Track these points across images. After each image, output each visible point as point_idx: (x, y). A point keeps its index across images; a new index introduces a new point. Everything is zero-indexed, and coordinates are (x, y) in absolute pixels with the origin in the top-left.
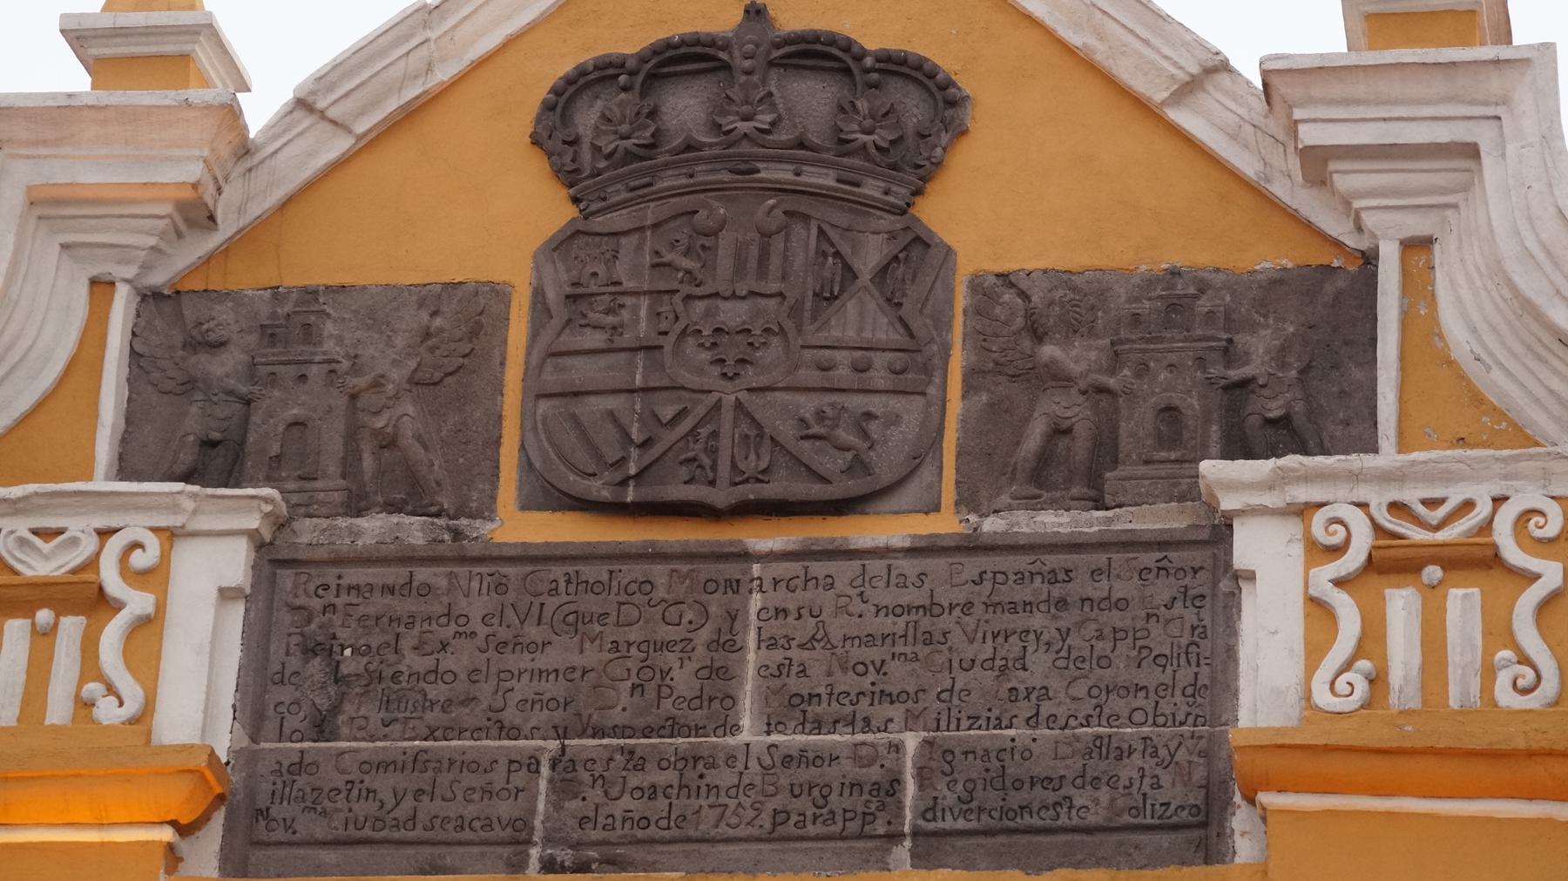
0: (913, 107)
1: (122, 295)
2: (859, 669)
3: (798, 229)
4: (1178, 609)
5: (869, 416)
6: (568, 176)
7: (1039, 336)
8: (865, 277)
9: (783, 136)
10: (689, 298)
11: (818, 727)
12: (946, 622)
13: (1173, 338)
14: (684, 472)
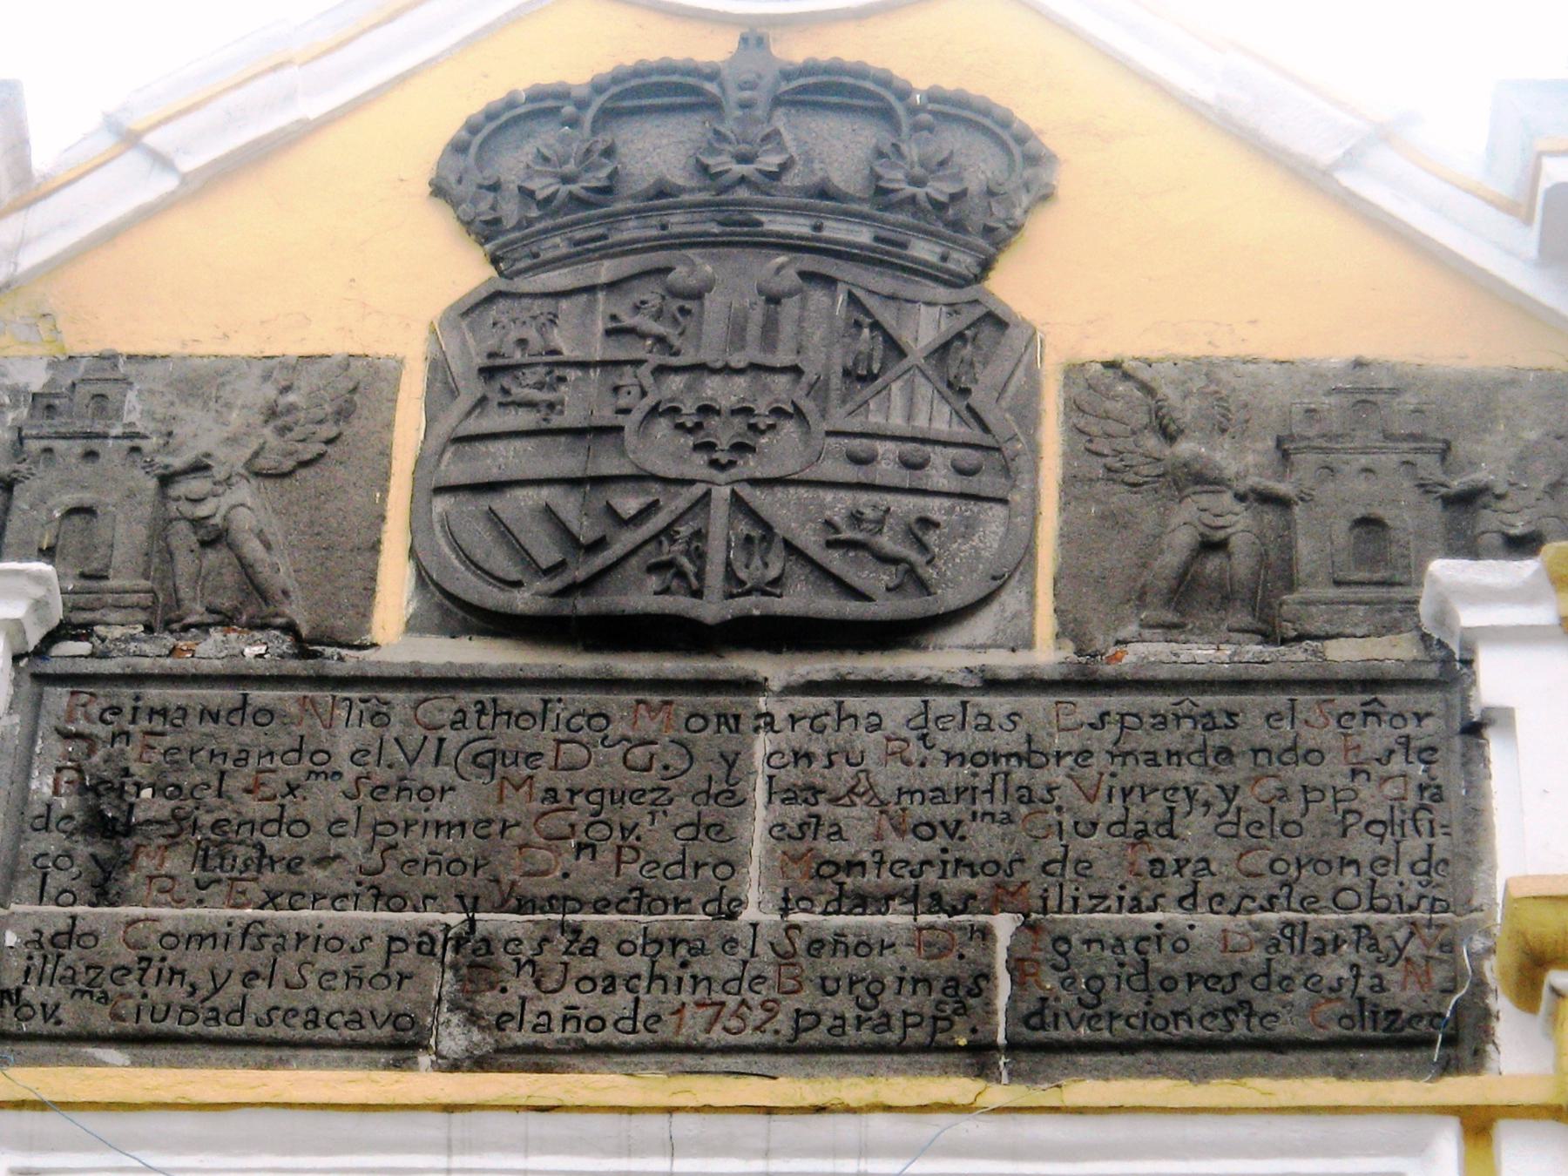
2: (925, 830)
4: (1397, 764)
5: (927, 523)
6: (485, 230)
7: (1169, 437)
11: (862, 902)
14: (654, 582)
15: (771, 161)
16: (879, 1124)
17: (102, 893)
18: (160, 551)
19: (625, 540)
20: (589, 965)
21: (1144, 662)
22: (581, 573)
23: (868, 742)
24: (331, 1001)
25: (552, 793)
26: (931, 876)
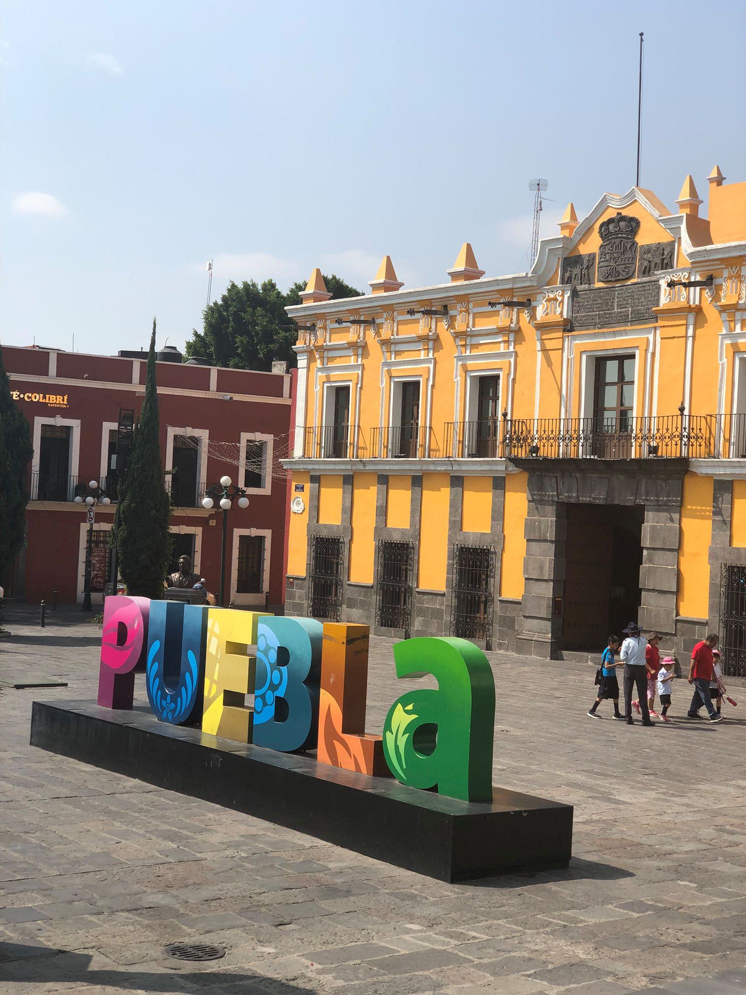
0: (634, 224)
8: (628, 248)
13: (724, 842)
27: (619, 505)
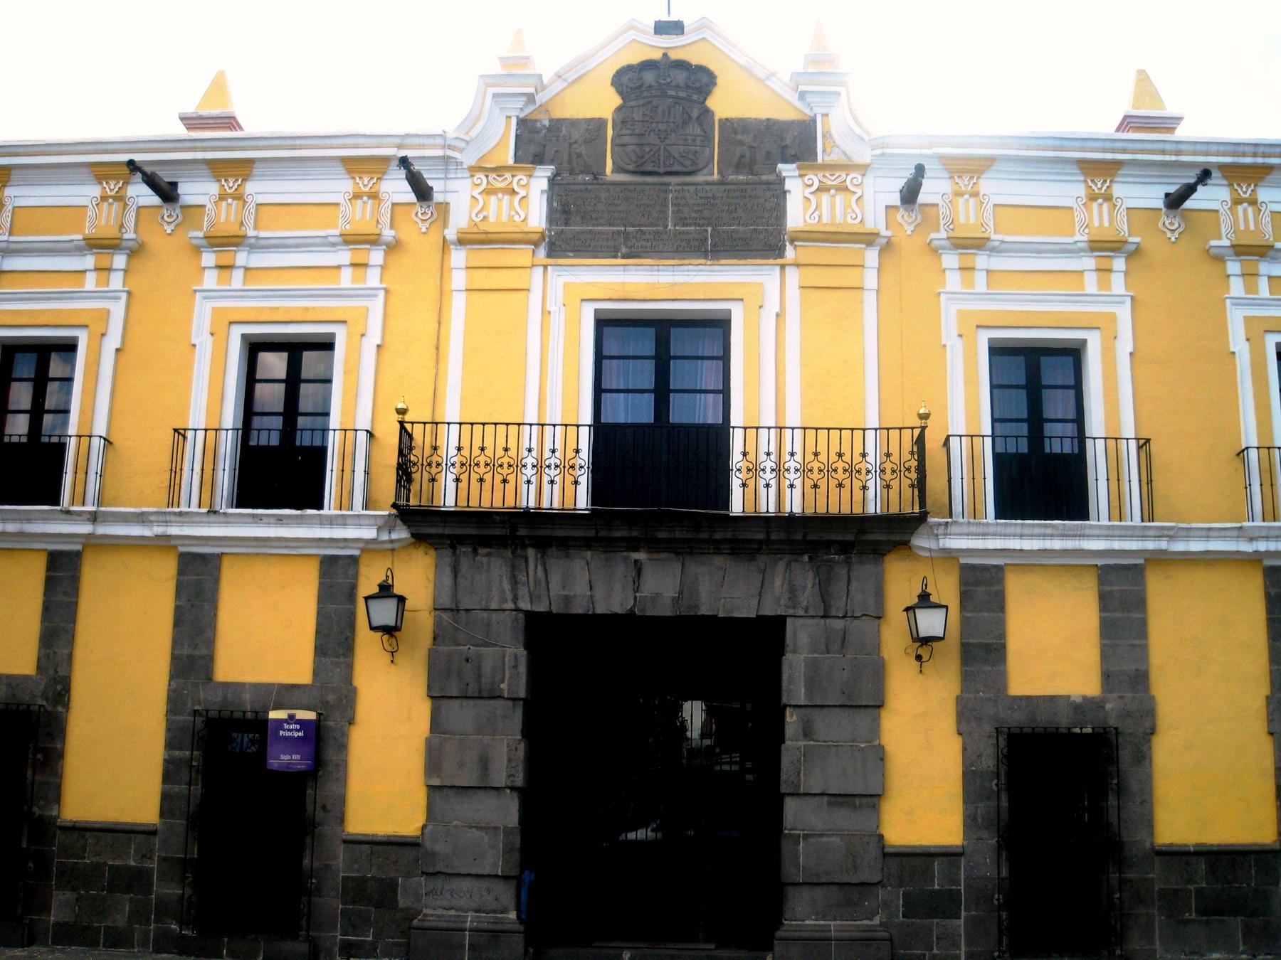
0: (705, 79)
1: (514, 121)
2: (696, 212)
3: (677, 106)
4: (772, 199)
5: (696, 152)
6: (620, 93)
7: (736, 134)
9: (673, 84)
10: (651, 123)
11: (687, 226)
12: (718, 201)
14: (652, 165)
15: (669, 80)
16: (691, 267)
17: (567, 224)
18: (570, 161)
19: (647, 156)
20: (645, 237)
21: (732, 180)
22: (640, 163)
23: (687, 195)
24: (605, 243)
25: (637, 205)
26: (698, 221)
27: (716, 616)
